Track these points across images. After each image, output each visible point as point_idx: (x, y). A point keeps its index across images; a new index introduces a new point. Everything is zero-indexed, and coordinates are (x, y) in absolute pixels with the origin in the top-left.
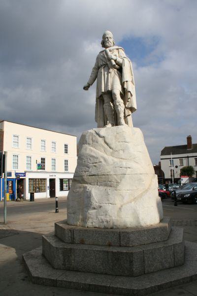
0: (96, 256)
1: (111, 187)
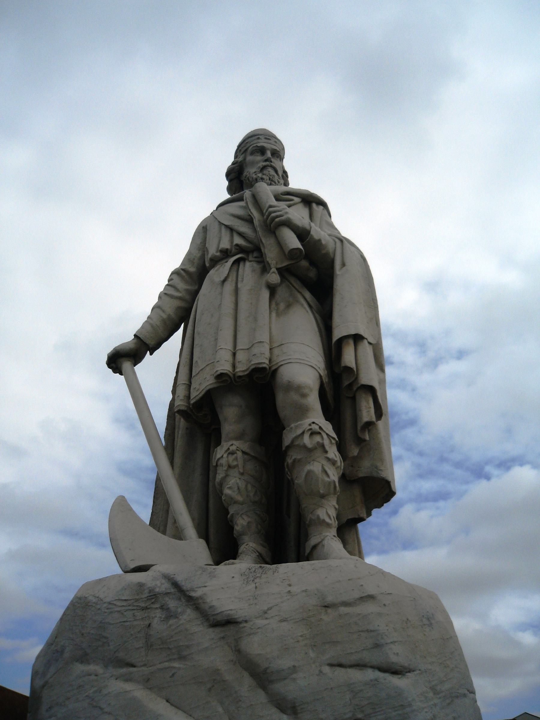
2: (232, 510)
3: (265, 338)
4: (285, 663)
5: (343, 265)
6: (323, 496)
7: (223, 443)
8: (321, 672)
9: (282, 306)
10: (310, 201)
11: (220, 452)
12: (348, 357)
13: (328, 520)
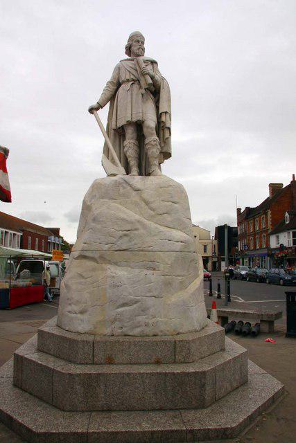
0: (144, 382)
1: (154, 269)
10: (153, 63)
11: (126, 143)
12: (163, 119)
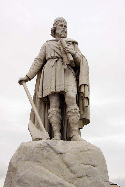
2: (53, 125)
3: (63, 84)
4: (72, 163)
5: (83, 64)
6: (76, 124)
7: (51, 108)
8: (80, 165)
9: (67, 74)
11: (50, 110)
12: (83, 90)
13: (77, 130)
